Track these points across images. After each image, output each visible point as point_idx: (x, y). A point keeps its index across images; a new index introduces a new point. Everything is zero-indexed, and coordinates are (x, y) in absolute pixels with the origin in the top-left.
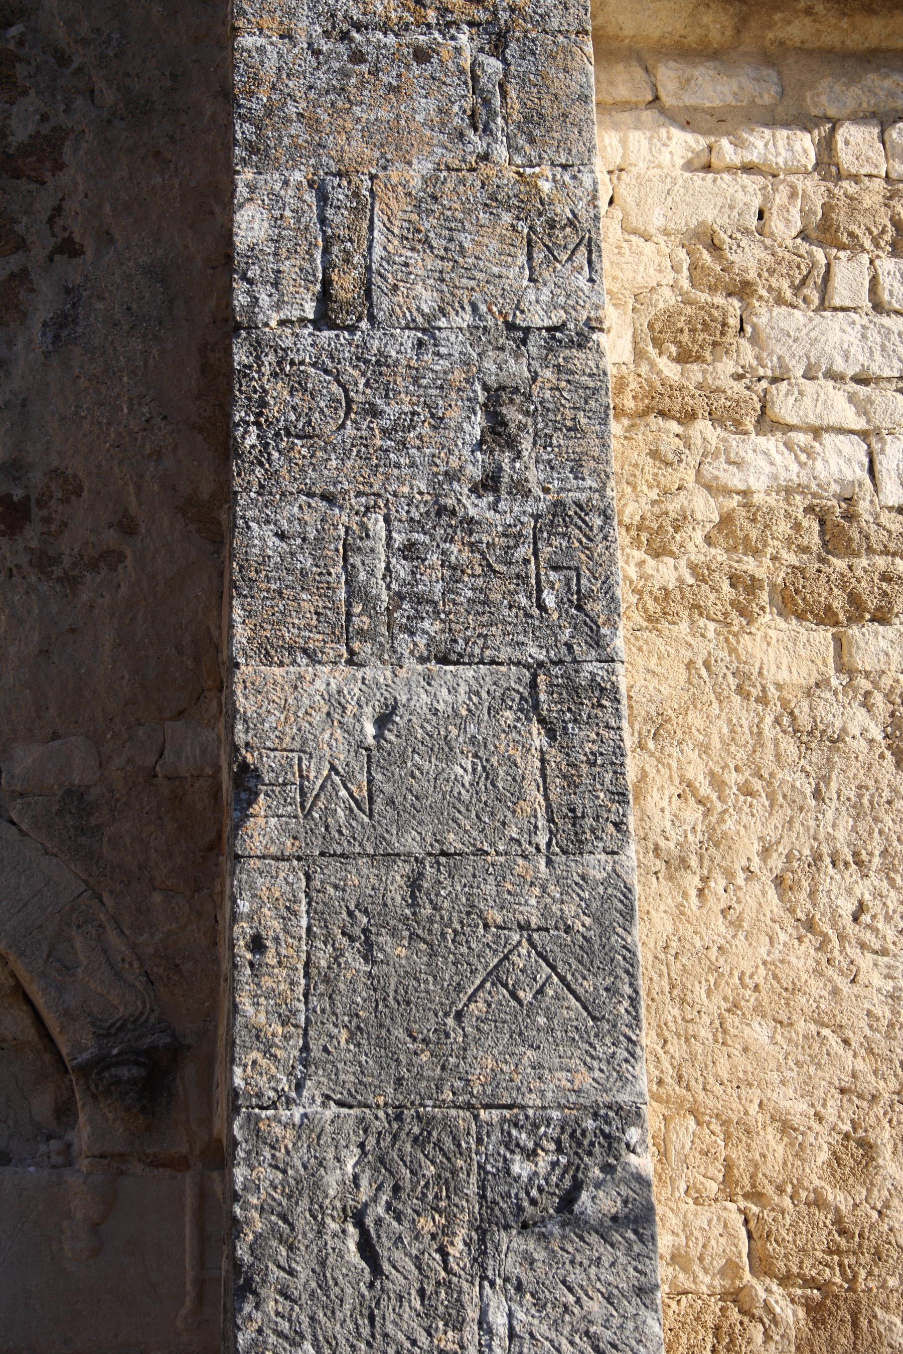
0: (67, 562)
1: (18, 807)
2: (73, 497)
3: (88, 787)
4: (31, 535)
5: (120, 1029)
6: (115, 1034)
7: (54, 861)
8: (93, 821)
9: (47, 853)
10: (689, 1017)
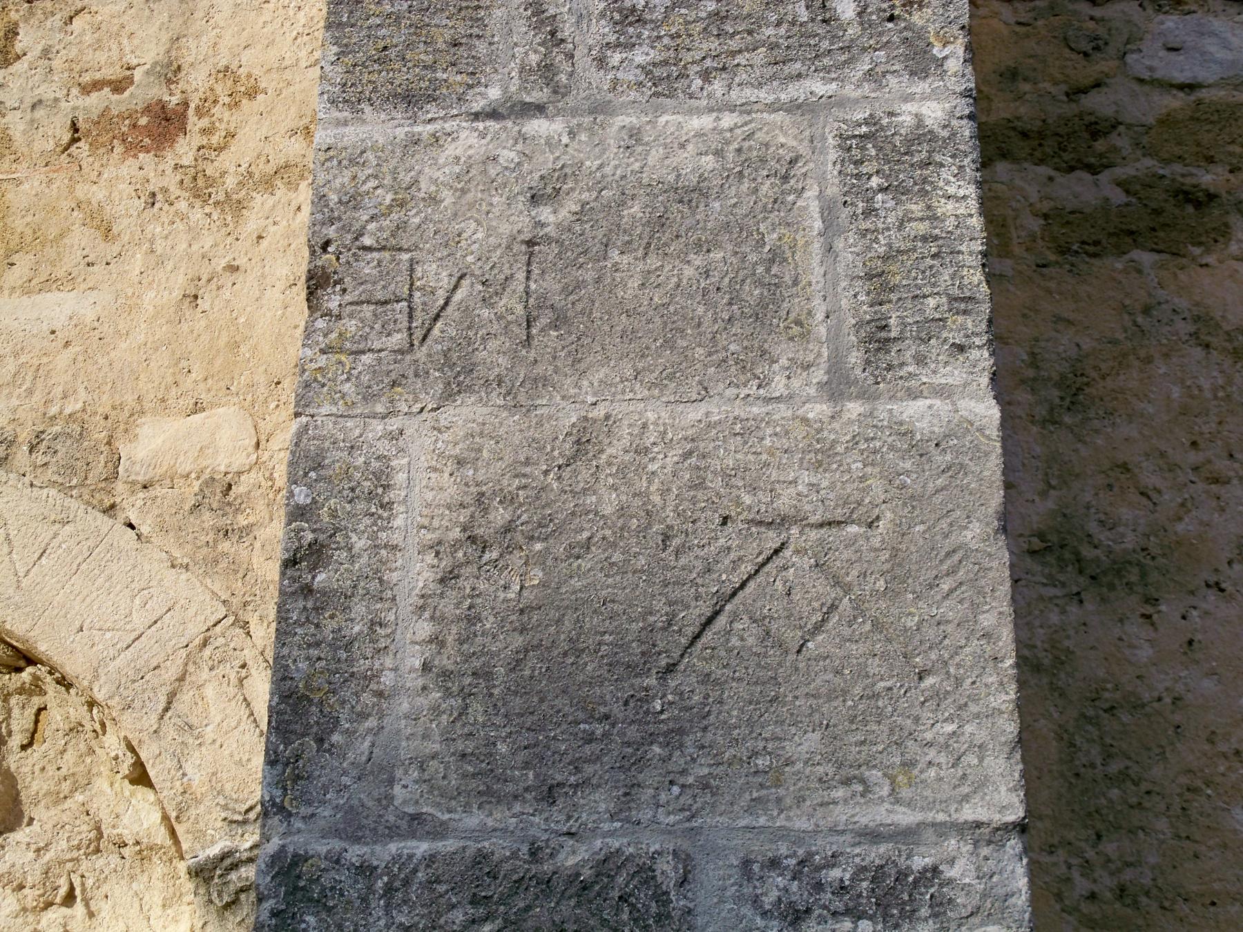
0: (230, 182)
1: (139, 503)
2: (244, 101)
3: (239, 473)
4: (185, 149)
7: (184, 577)
8: (242, 521)
9: (173, 566)
10: (1134, 800)
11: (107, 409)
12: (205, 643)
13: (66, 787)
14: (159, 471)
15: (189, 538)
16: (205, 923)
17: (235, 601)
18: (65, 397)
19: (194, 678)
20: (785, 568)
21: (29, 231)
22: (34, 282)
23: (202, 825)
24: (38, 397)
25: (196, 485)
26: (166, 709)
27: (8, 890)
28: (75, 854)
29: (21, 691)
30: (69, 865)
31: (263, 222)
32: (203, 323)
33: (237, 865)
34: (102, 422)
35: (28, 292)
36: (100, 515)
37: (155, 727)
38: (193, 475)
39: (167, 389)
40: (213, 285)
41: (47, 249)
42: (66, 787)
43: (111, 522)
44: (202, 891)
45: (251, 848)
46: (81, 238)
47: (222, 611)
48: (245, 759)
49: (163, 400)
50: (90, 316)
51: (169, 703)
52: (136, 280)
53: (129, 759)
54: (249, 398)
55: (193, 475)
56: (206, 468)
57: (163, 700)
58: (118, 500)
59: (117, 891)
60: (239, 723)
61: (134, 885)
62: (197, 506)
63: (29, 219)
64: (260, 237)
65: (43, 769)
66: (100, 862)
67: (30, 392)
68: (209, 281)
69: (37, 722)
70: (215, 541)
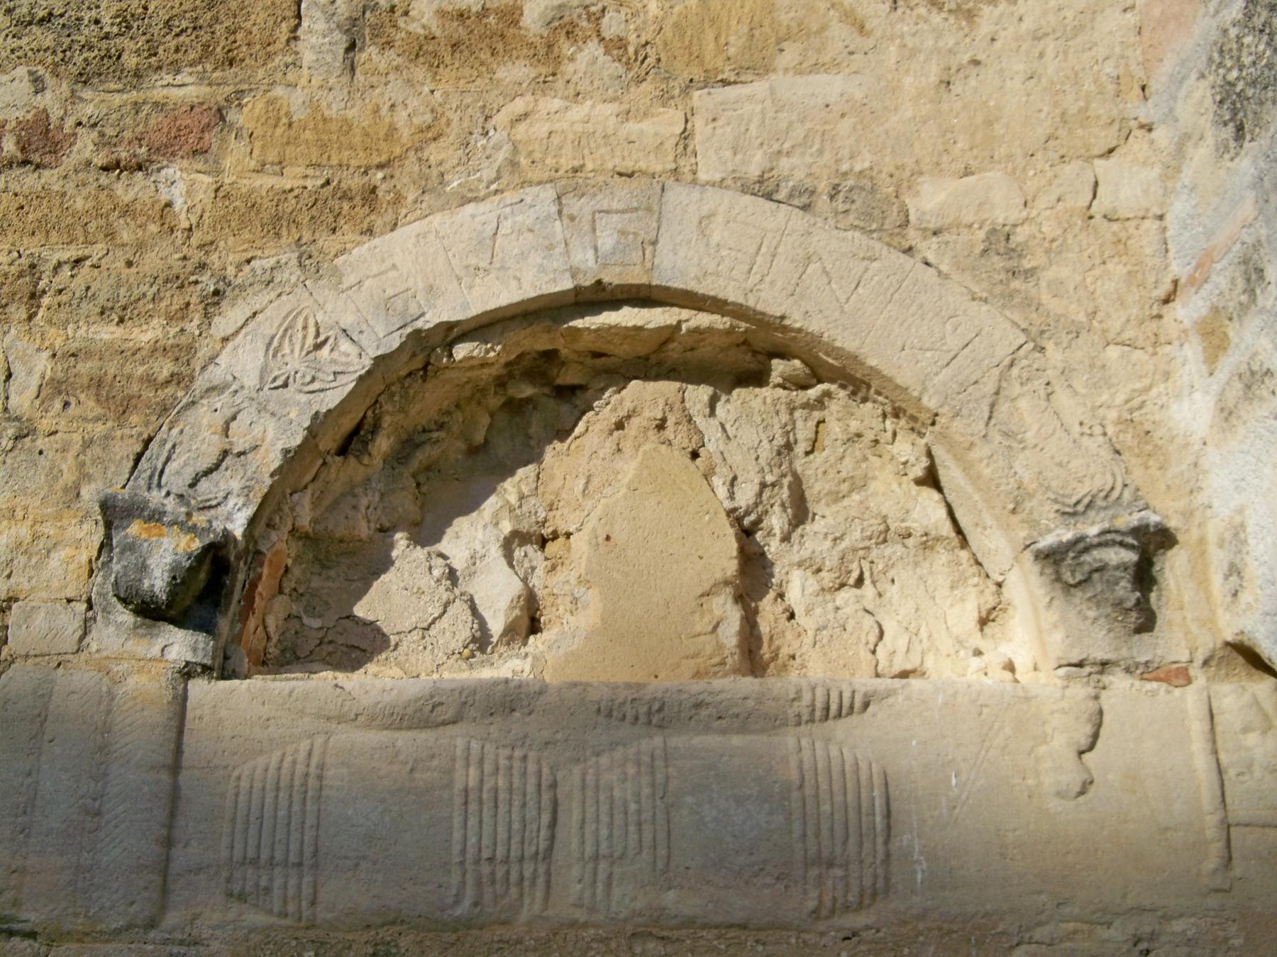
1: (934, 246)
3: (1015, 226)
5: (1088, 506)
6: (1084, 512)
7: (985, 308)
9: (974, 299)
11: (892, 169)
12: (1012, 365)
13: (845, 487)
14: (948, 221)
15: (984, 275)
17: (1034, 330)
18: (851, 158)
19: (1007, 393)
21: (793, 24)
22: (804, 65)
23: (1036, 516)
24: (827, 157)
25: (981, 234)
26: (990, 418)
27: (809, 573)
28: (867, 543)
29: (806, 406)
30: (861, 553)
31: (993, 28)
32: (959, 105)
34: (888, 179)
35: (800, 73)
36: (902, 256)
37: (983, 432)
38: (976, 226)
39: (940, 155)
40: (961, 74)
41: (812, 39)
42: (845, 487)
43: (912, 261)
44: (1049, 571)
46: (839, 33)
47: (1022, 339)
48: (1066, 460)
49: (938, 164)
50: (858, 95)
51: (991, 412)
52: (894, 67)
53: (925, 462)
54: (1010, 165)
55: (976, 226)
56: (986, 220)
57: (986, 409)
58: (913, 243)
60: (1055, 431)
62: (985, 251)
63: (792, 14)
64: (993, 40)
65: (825, 472)
66: (888, 550)
67: (820, 152)
68: (958, 70)
69: (817, 432)
70: (1008, 280)
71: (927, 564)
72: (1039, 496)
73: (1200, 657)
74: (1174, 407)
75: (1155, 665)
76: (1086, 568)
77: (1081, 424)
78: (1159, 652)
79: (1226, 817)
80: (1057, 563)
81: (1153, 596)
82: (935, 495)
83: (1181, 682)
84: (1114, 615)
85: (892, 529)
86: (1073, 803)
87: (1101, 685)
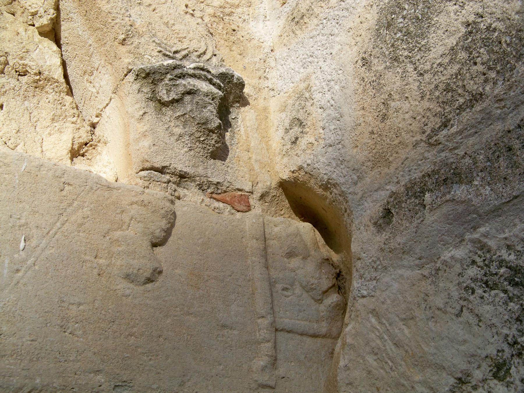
16: (145, 113)
20: (488, 42)
33: (184, 76)
45: (194, 68)
48: (172, 22)
59: (13, 103)
61: (26, 103)
71: (35, 100)
72: (146, 37)
73: (259, 190)
74: (252, 24)
75: (224, 188)
76: (181, 89)
77: (187, 6)
78: (229, 178)
79: (274, 321)
80: (154, 83)
81: (228, 135)
82: (55, 47)
83: (242, 208)
84: (198, 135)
85: (11, 63)
86: (142, 288)
87: (176, 194)
